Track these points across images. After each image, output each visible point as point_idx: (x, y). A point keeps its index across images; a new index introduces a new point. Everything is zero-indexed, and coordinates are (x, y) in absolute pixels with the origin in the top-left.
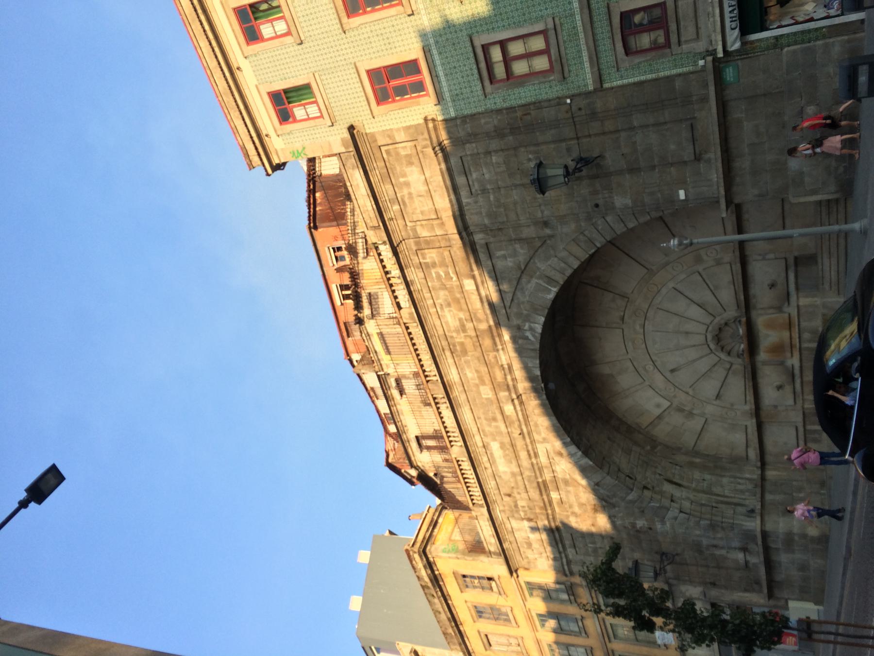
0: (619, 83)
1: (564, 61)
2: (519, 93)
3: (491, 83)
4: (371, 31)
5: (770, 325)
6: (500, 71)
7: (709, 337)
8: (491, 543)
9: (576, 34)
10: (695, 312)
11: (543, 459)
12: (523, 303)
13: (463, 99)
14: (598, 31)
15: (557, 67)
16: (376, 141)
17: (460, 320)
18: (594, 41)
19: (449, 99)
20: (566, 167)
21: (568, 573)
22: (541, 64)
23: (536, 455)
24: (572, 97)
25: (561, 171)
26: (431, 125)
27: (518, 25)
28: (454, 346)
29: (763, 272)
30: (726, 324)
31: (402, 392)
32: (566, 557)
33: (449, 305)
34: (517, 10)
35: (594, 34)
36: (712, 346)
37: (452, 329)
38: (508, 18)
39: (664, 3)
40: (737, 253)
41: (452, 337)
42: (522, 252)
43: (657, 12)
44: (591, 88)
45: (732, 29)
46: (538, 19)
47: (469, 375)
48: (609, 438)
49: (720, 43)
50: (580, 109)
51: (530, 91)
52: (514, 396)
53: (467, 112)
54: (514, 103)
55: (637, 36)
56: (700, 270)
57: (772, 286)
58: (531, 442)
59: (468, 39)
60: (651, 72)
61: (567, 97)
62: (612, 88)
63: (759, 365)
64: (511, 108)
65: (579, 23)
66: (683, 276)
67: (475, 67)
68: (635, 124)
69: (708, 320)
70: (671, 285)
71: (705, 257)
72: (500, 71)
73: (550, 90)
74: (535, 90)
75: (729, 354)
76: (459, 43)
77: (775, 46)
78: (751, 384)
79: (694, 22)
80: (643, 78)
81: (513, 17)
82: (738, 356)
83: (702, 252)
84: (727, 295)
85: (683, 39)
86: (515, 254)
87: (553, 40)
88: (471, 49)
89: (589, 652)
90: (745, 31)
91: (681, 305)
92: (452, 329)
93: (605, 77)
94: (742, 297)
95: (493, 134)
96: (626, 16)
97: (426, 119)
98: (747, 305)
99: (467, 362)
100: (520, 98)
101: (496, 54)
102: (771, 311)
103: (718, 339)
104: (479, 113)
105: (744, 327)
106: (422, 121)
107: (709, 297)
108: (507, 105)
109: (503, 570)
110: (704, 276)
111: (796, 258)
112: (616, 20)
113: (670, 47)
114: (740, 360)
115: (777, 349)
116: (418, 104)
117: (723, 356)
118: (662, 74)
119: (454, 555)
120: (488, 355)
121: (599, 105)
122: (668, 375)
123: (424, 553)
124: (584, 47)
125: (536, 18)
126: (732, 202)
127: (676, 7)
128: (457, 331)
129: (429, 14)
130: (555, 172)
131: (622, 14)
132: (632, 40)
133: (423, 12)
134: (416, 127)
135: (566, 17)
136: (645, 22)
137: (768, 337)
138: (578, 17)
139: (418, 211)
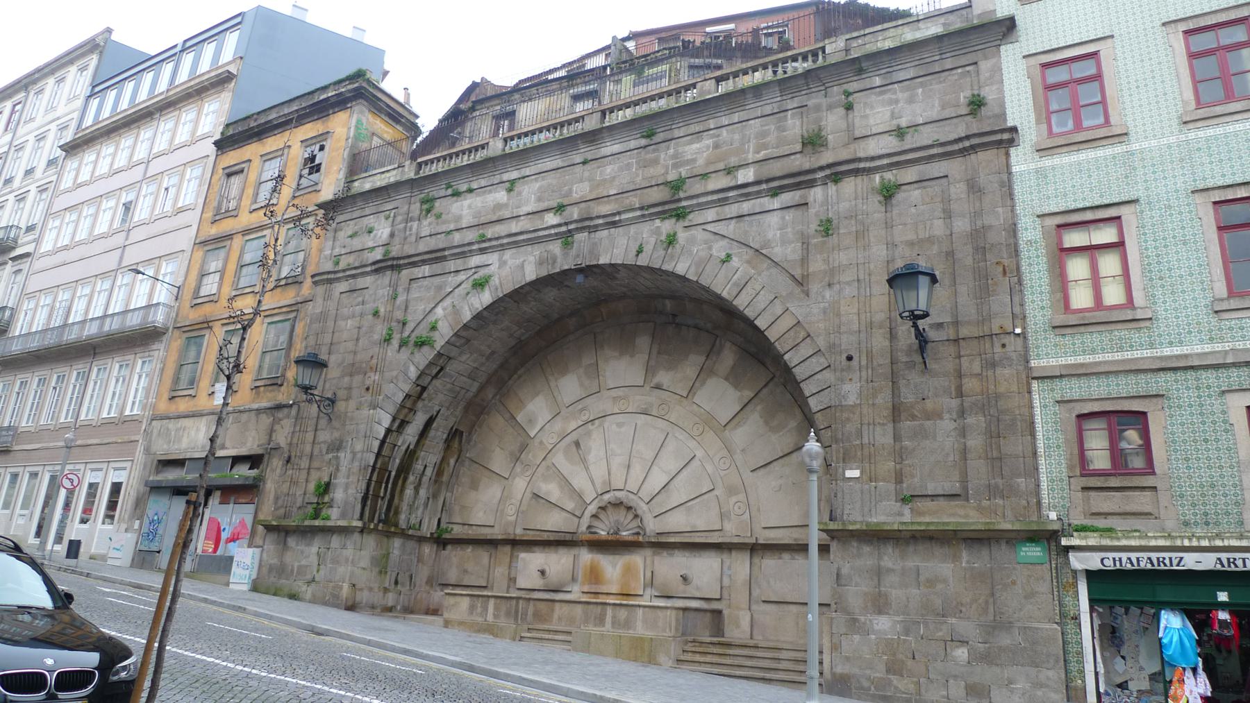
0: (1037, 403)
1: (1082, 329)
2: (1038, 264)
3: (1059, 226)
4: (1160, 63)
5: (628, 571)
6: (1074, 239)
7: (618, 494)
8: (364, 184)
9: (1121, 349)
10: (657, 479)
11: (475, 260)
12: (710, 248)
13: (1038, 185)
14: (1122, 380)
15: (1073, 319)
16: (986, 58)
17: (694, 160)
18: (1107, 373)
19: (1040, 164)
20: (925, 315)
21: (317, 278)
22: (1081, 298)
23: (482, 251)
24: (1023, 336)
25: (923, 306)
26: (1006, 136)
27: (1146, 270)
28: (654, 151)
29: (705, 572)
30: (636, 516)
31: (577, 98)
32: (338, 280)
33: (716, 146)
34: (1170, 270)
35: (1116, 373)
36: (606, 497)
37: (680, 149)
38: (1157, 256)
39: (1154, 473)
40: (736, 540)
41: (668, 148)
42: (787, 252)
43: (1138, 463)
44: (1033, 363)
45: (1102, 560)
46: (1150, 297)
47: (609, 169)
48: (493, 353)
49: (1083, 543)
50: (1004, 346)
51: (1040, 278)
52: (572, 227)
53: (1017, 189)
54: (1024, 254)
55: (1106, 433)
56: (715, 492)
57: (685, 579)
58: (502, 245)
59: (1133, 198)
60: (1047, 447)
61: (1024, 328)
62: (1030, 392)
63: (575, 551)
64: (1016, 251)
65: (1137, 354)
66: (710, 468)
67: (1088, 205)
68: (970, 420)
69: (646, 493)
70: (700, 454)
71: (734, 499)
72: (1074, 239)
73: (1038, 302)
74: (1040, 286)
75: (595, 516)
76: (1128, 184)
77: (1063, 615)
78: (552, 538)
79: (1118, 510)
80: (1039, 435)
81: (1159, 263)
82: (589, 527)
83: (742, 497)
84: (677, 522)
85: (1093, 494)
86: (784, 242)
87: (1115, 316)
88: (1117, 200)
89: (211, 298)
90: (1091, 575)
91: (669, 463)
92: (680, 149)
93: (1047, 385)
94: (672, 540)
95: (979, 223)
96: (1139, 419)
97: (1014, 130)
98: (661, 545)
99: (629, 166)
100: (1030, 265)
101: (1106, 235)
102: (649, 574)
103: (618, 504)
104: (1013, 206)
105: (631, 538)
106: (1010, 124)
107: (677, 496)
108: (1022, 245)
109: (327, 194)
110: (705, 497)
111: (720, 612)
112: (1136, 406)
113: (1082, 475)
114: (583, 528)
115: (594, 575)
116: (1038, 122)
117: (592, 509)
118: (1042, 461)
119: (352, 135)
120: (635, 196)
121: (1004, 372)
122: (574, 436)
123: (359, 94)
124: (1099, 358)
125: (1154, 296)
126: (833, 538)
127: (1143, 488)
128: (675, 156)
129: (1178, 146)
130: (921, 297)
131: (1144, 414)
132: (1101, 424)
133: (1183, 137)
134: (1003, 116)
135: (1150, 337)
136: (1123, 445)
137: (612, 567)
138: (1147, 353)
139: (868, 111)
